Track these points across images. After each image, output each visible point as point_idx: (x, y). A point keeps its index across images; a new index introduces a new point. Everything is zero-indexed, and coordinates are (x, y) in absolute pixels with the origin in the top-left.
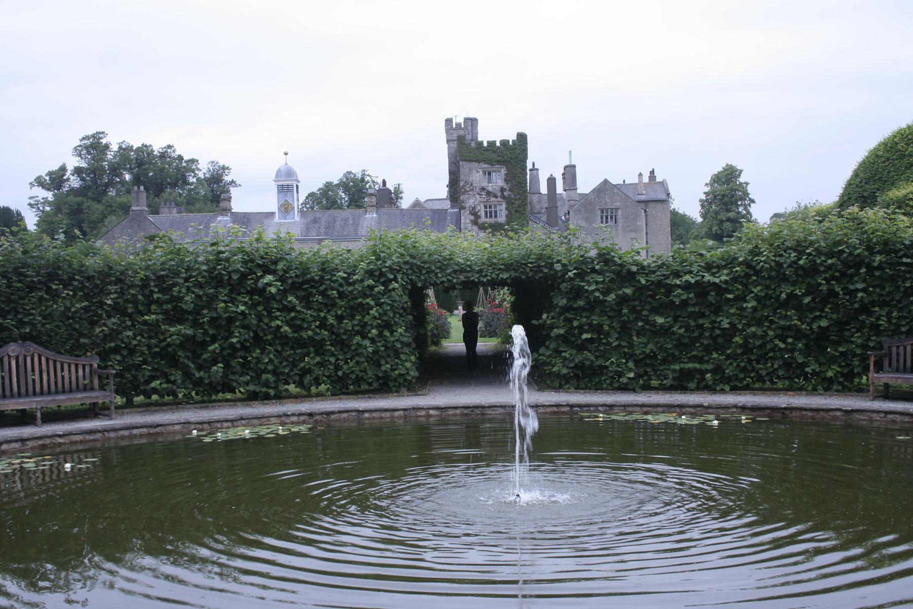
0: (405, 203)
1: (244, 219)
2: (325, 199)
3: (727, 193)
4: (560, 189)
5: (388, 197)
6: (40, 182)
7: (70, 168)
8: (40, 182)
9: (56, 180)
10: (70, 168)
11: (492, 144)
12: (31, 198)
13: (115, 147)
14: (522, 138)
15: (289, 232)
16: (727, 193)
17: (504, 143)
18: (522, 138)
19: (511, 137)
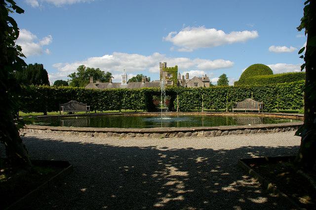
0: (151, 81)
1: (115, 85)
2: (133, 80)
3: (223, 80)
4: (185, 78)
5: (148, 80)
6: (70, 76)
7: (76, 73)
8: (70, 76)
9: (73, 75)
10: (76, 73)
11: (31, 65)
12: (300, 52)
13: (86, 68)
14: (177, 67)
15: (124, 85)
16: (223, 80)
17: (173, 68)
18: (177, 67)
19: (174, 67)
